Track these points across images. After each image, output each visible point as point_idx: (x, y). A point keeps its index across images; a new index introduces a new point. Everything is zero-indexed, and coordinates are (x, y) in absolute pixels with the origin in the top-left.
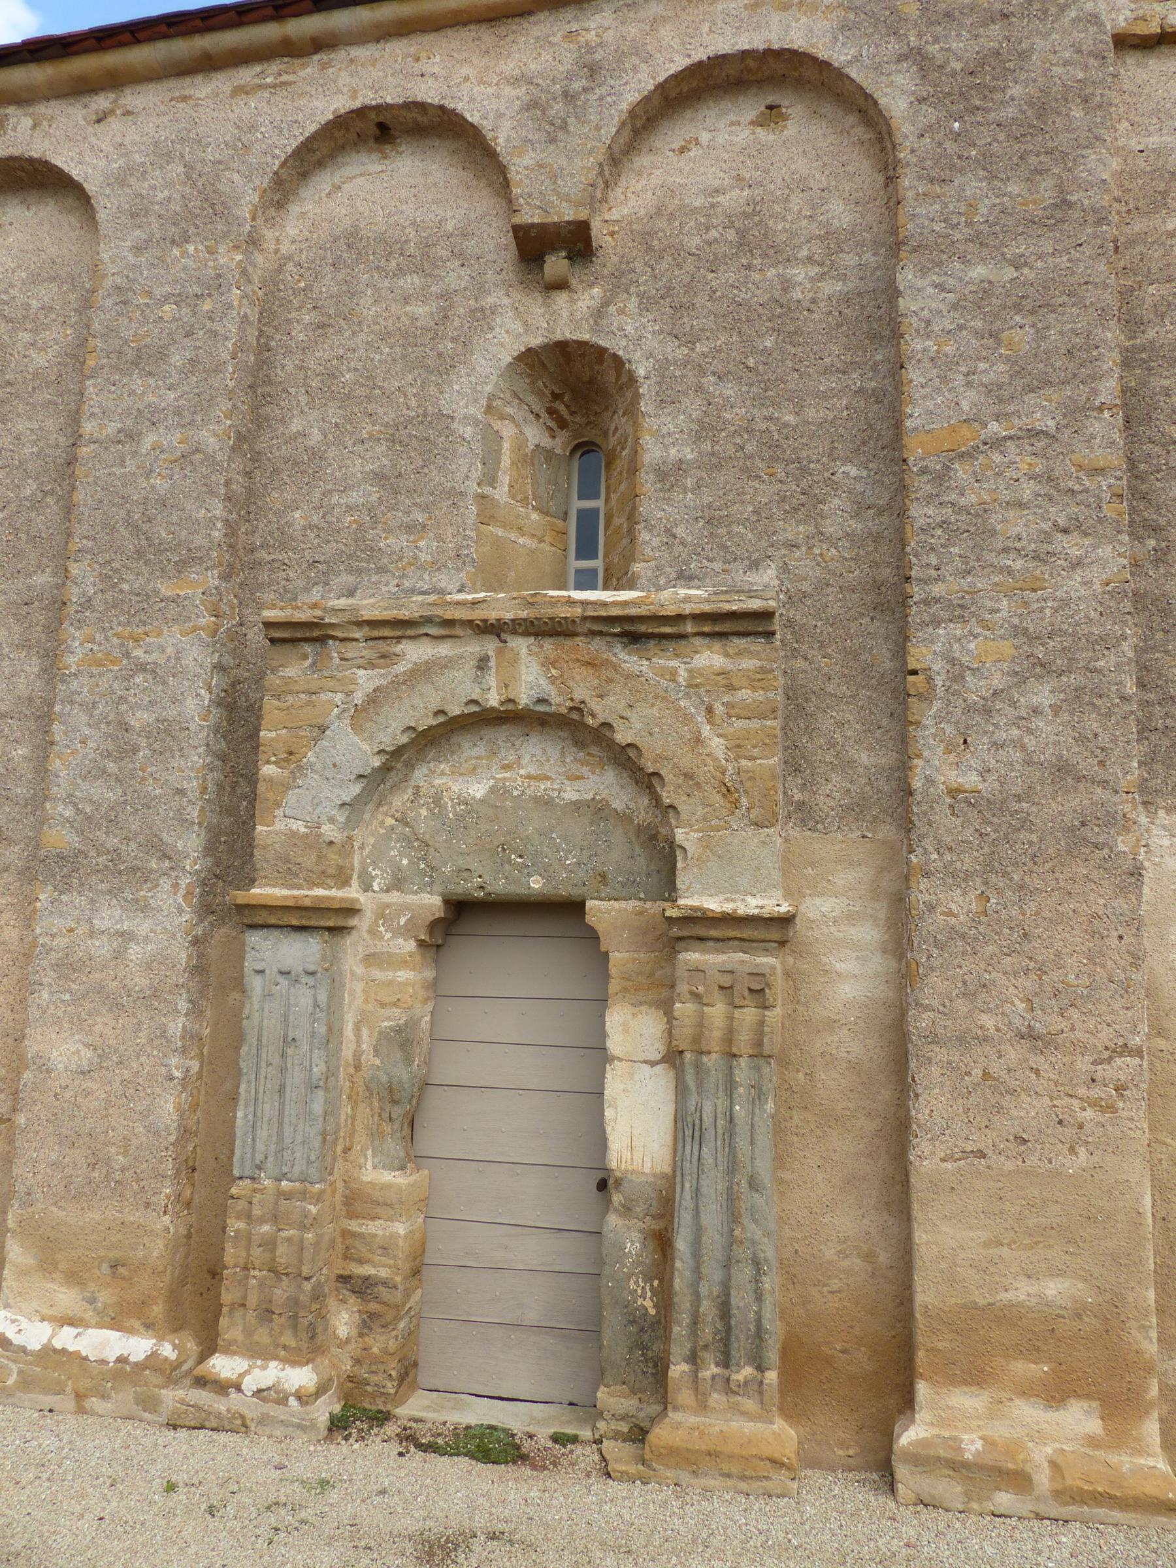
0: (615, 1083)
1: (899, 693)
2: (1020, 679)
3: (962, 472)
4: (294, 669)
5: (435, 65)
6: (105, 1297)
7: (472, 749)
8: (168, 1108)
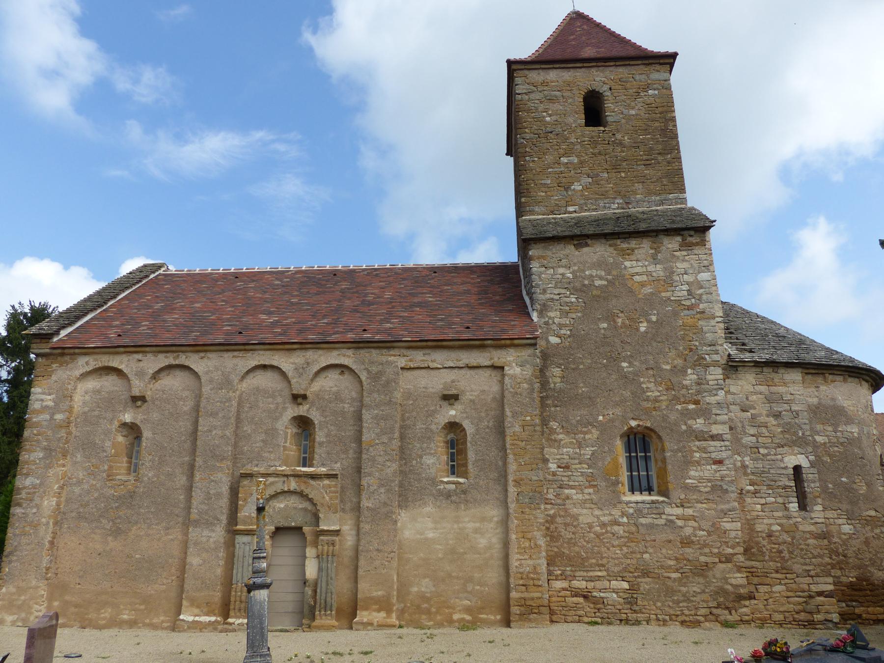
0: (307, 562)
1: (359, 489)
2: (379, 487)
3: (371, 449)
4: (246, 482)
5: (276, 357)
6: (205, 610)
7: (281, 498)
8: (219, 571)
